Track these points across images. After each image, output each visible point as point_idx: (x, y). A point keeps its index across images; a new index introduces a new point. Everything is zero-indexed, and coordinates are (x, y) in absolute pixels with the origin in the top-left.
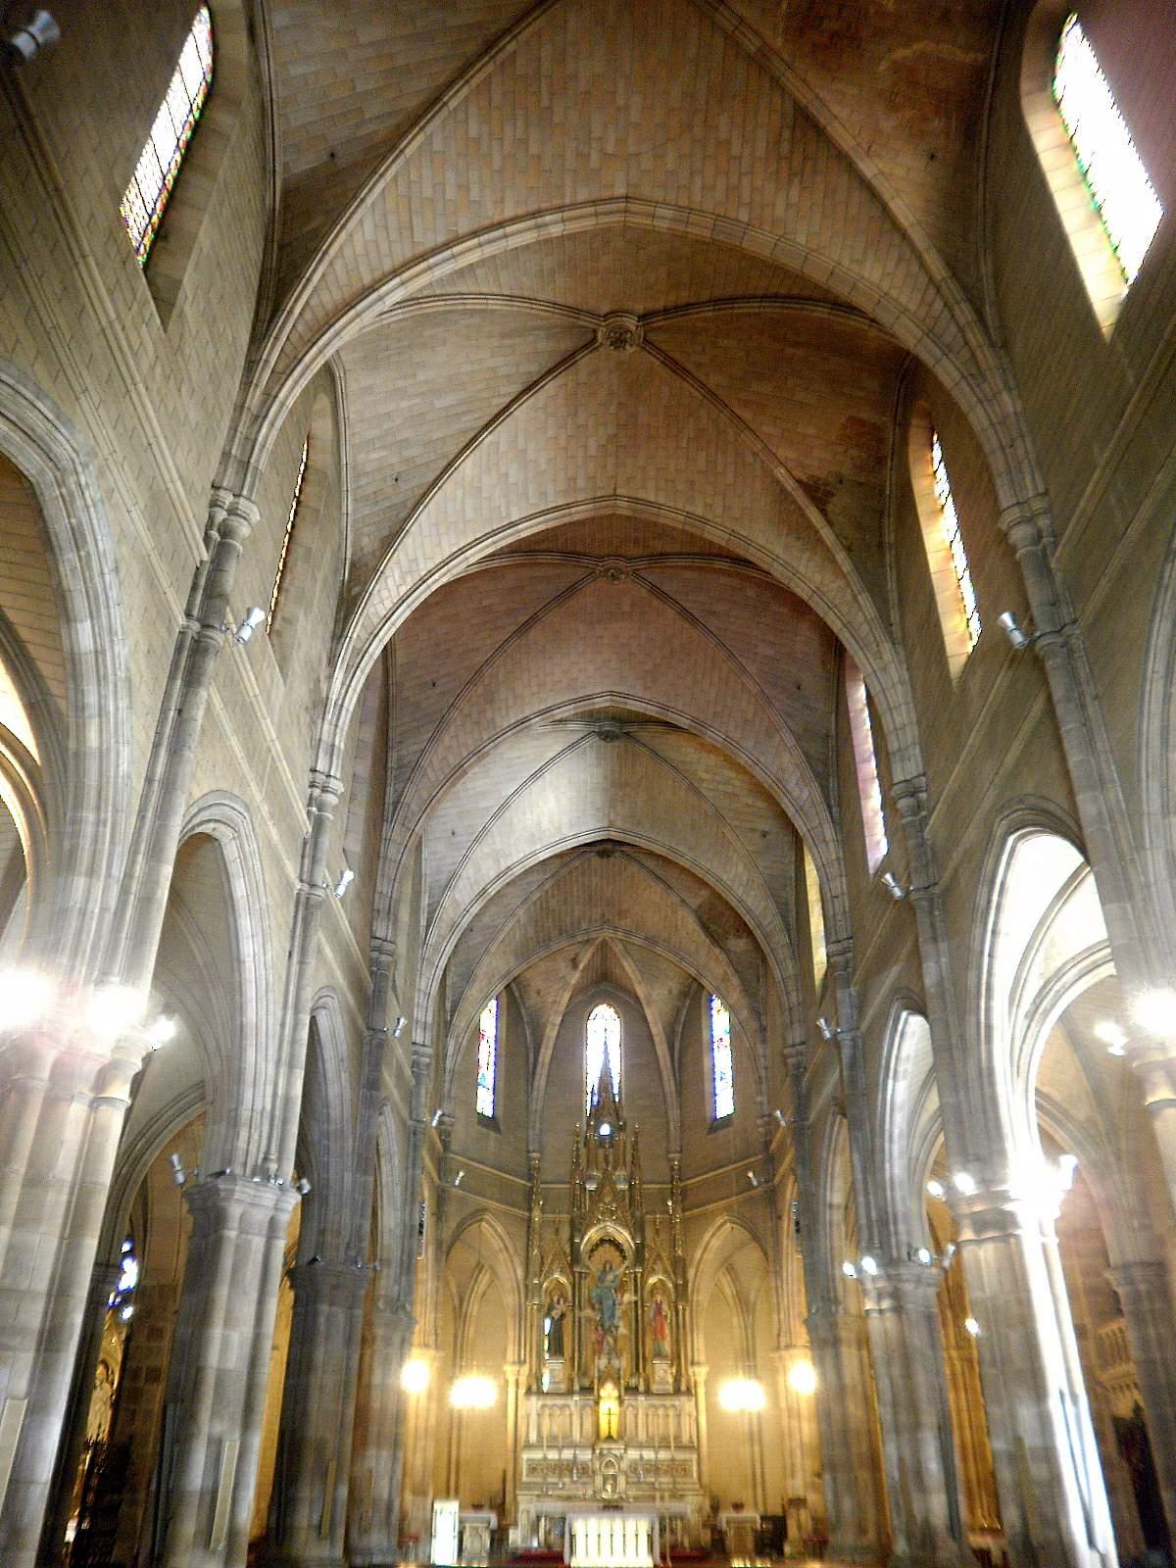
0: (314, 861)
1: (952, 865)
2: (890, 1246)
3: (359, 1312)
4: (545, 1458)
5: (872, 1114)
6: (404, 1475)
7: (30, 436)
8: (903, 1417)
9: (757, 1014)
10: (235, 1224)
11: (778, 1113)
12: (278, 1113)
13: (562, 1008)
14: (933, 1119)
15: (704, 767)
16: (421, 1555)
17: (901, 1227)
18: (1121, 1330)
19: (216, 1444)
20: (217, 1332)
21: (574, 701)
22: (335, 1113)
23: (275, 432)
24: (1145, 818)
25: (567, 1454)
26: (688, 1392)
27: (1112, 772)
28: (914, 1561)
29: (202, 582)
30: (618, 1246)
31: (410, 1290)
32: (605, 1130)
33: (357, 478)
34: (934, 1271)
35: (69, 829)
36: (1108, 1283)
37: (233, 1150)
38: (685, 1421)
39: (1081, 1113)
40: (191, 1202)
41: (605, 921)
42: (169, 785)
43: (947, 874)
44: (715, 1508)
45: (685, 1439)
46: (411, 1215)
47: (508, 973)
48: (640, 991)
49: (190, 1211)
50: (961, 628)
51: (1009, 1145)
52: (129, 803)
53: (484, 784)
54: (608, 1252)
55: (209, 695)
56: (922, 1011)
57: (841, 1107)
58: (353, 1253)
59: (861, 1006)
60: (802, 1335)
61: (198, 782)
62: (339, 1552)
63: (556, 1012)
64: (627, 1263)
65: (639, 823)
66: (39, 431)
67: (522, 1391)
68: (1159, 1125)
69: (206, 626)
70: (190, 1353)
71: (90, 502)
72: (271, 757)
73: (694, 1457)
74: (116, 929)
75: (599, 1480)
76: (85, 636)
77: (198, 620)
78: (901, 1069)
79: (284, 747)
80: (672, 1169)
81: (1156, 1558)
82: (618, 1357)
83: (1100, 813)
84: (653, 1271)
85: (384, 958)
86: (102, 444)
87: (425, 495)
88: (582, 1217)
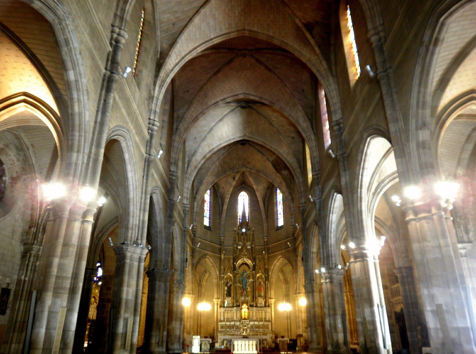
0: (150, 147)
1: (350, 148)
2: (330, 264)
3: (168, 284)
4: (226, 324)
5: (325, 225)
6: (184, 328)
7: (49, 8)
8: (331, 312)
9: (291, 194)
10: (129, 258)
11: (297, 224)
12: (141, 225)
13: (230, 193)
14: (344, 227)
15: (274, 117)
16: (189, 351)
17: (333, 258)
18: (398, 287)
19: (126, 320)
20: (125, 289)
21: (232, 96)
22: (159, 225)
23: (131, 7)
24: (410, 131)
25: (232, 323)
26: (269, 306)
27: (400, 117)
28: (334, 352)
29: (110, 58)
30: (246, 264)
31: (184, 278)
32: (244, 230)
33: (161, 23)
34: (342, 270)
35: (70, 138)
36: (394, 273)
37: (127, 236)
38: (267, 314)
39: (389, 223)
40: (115, 252)
41: (243, 165)
42: (102, 124)
43: (349, 150)
44: (276, 337)
45: (267, 319)
46: (184, 255)
47: (214, 181)
48: (255, 187)
49: (115, 254)
50: (355, 70)
51: (366, 234)
52: (89, 130)
53: (204, 123)
54: (245, 267)
55: (114, 95)
56: (340, 192)
57: (316, 222)
58: (165, 267)
59: (322, 191)
60: (303, 290)
61: (112, 123)
62: (164, 350)
63: (229, 194)
64: (250, 270)
65: (254, 135)
66: (52, 6)
67: (219, 306)
68: (410, 227)
69: (112, 73)
70: (118, 294)
71: (70, 30)
72: (135, 118)
73: (270, 323)
74: (87, 169)
75: (242, 330)
76: (71, 76)
77: (109, 71)
78: (334, 211)
79: (140, 111)
80: (264, 242)
81: (405, 351)
82: (247, 297)
83: (396, 130)
84: (258, 273)
85: (174, 178)
86: (73, 10)
87: (183, 29)
88: (237, 256)
